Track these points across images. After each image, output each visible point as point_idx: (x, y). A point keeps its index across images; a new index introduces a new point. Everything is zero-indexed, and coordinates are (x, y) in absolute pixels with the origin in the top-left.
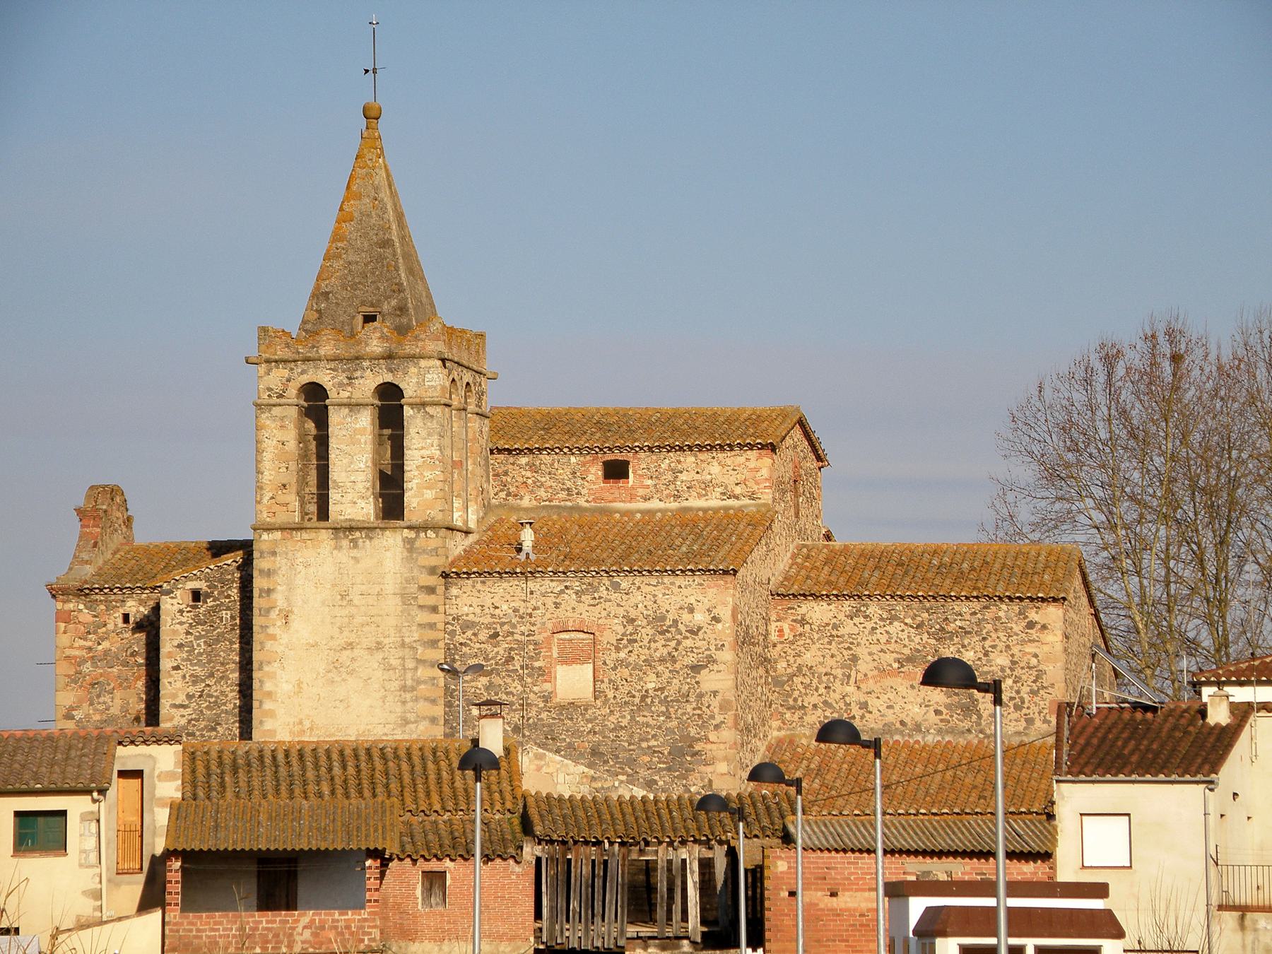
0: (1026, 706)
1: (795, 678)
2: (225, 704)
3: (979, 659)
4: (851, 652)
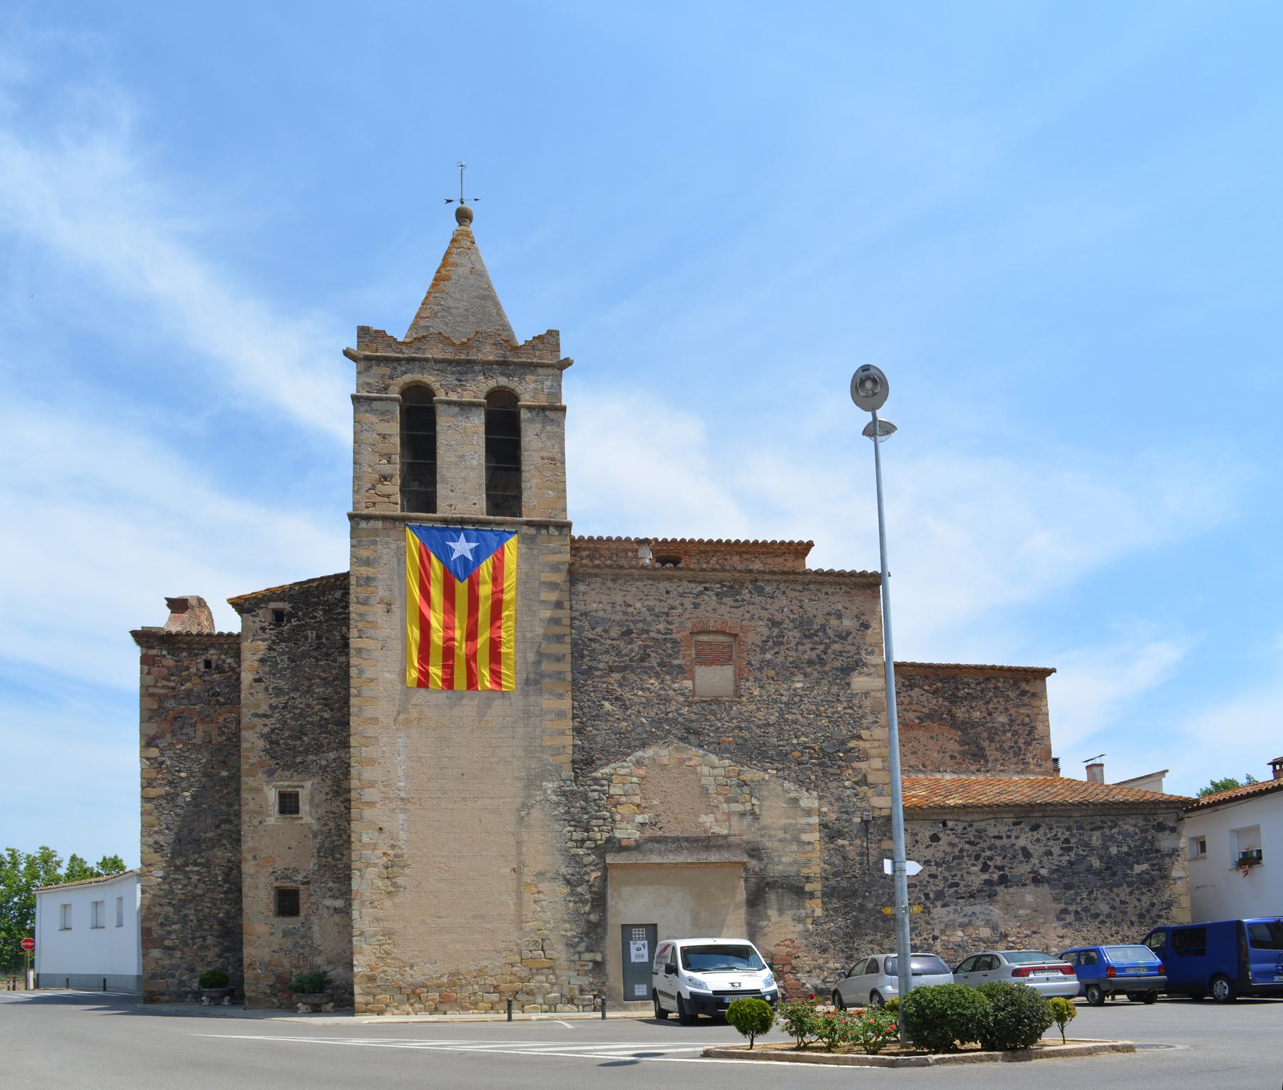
0: (1022, 752)
2: (310, 716)
3: (984, 717)
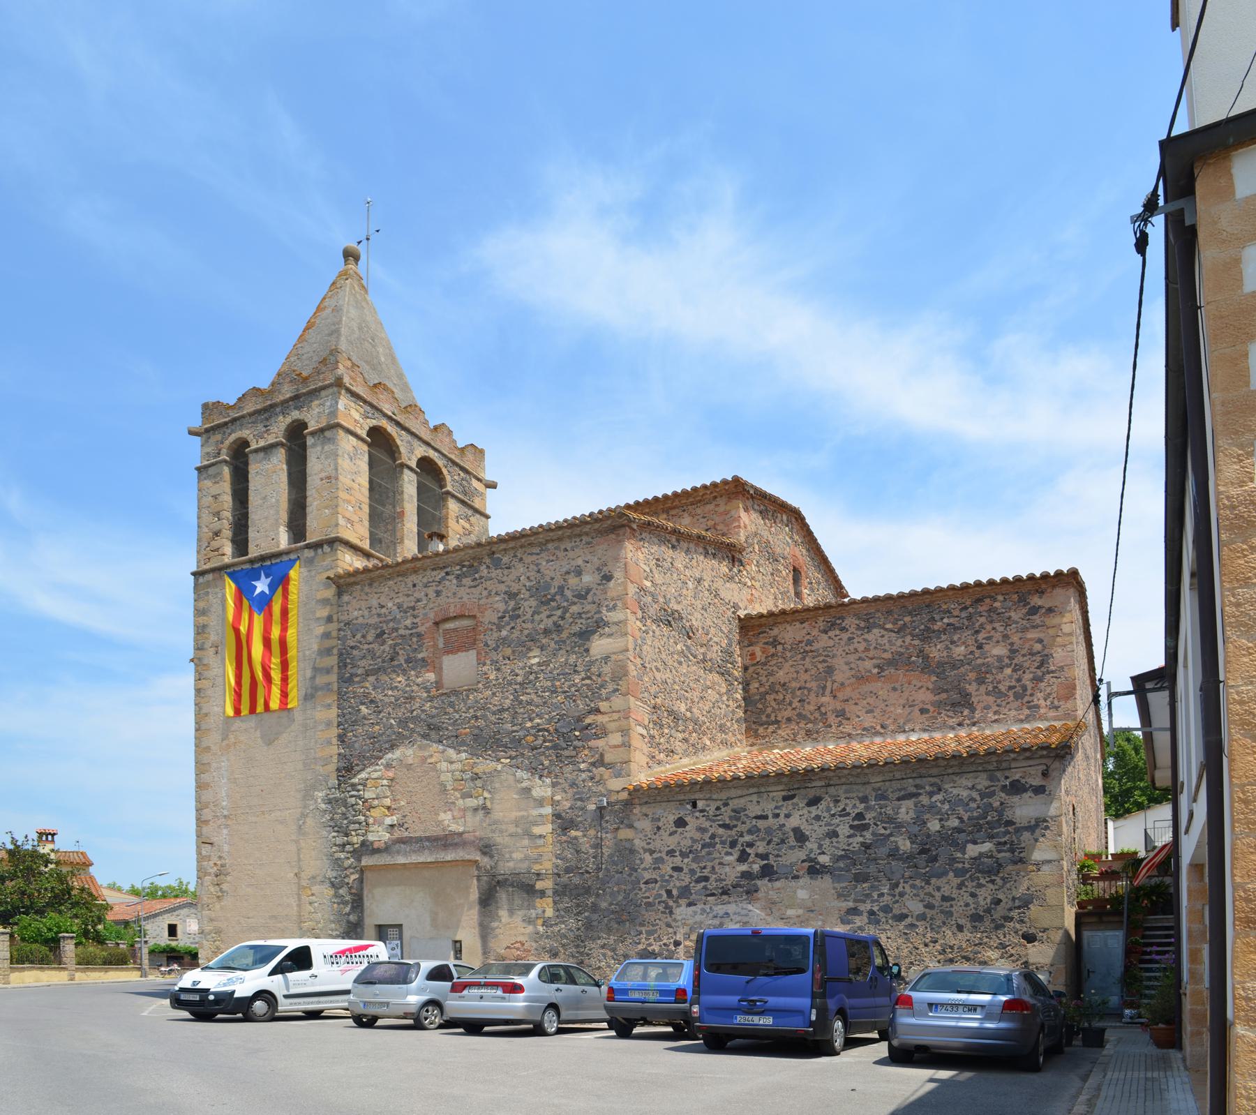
0: (1029, 692)
1: (767, 697)
3: (972, 653)
4: (826, 665)
